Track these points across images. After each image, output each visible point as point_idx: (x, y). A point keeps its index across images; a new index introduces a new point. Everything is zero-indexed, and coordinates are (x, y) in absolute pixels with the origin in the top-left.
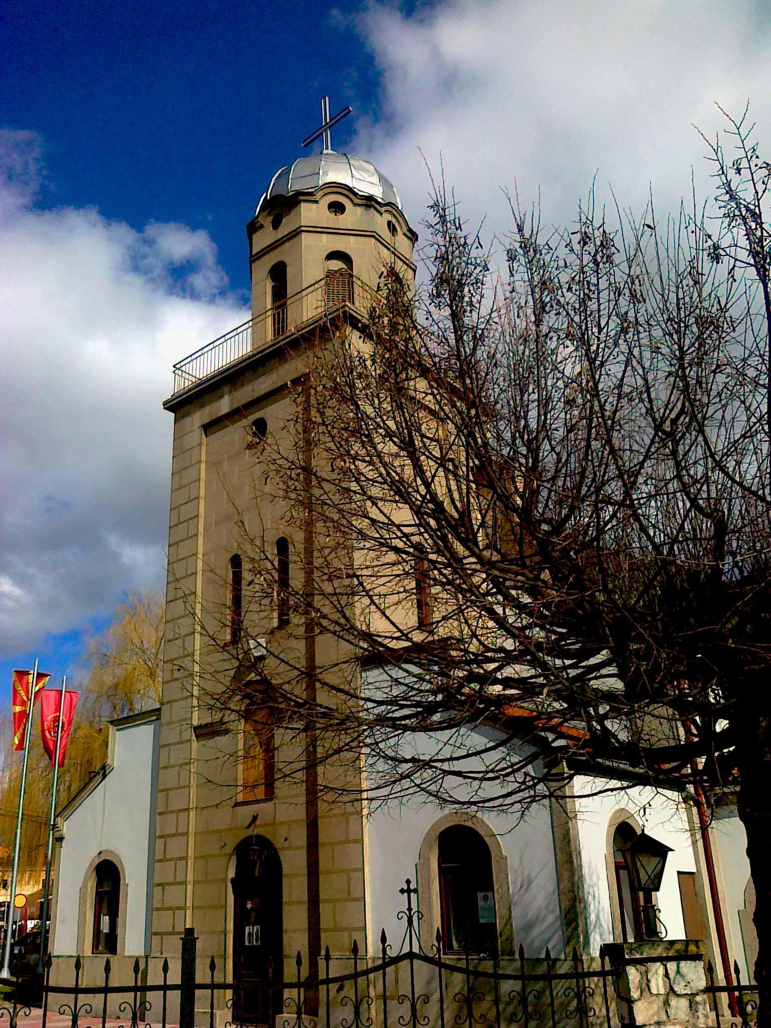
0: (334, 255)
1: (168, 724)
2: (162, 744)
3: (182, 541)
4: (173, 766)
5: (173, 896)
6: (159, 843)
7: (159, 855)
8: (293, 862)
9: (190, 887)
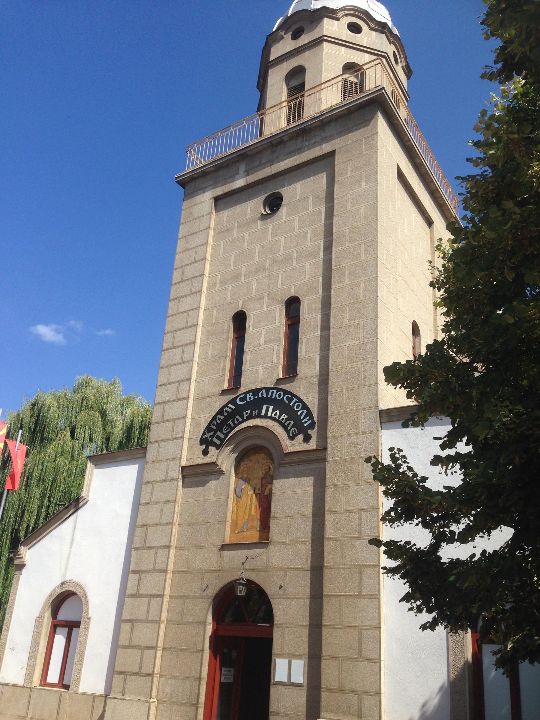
0: (350, 67)
1: (154, 462)
2: (144, 481)
3: (186, 296)
4: (156, 503)
5: (143, 634)
6: (133, 579)
7: (130, 590)
8: (289, 615)
9: (163, 627)
